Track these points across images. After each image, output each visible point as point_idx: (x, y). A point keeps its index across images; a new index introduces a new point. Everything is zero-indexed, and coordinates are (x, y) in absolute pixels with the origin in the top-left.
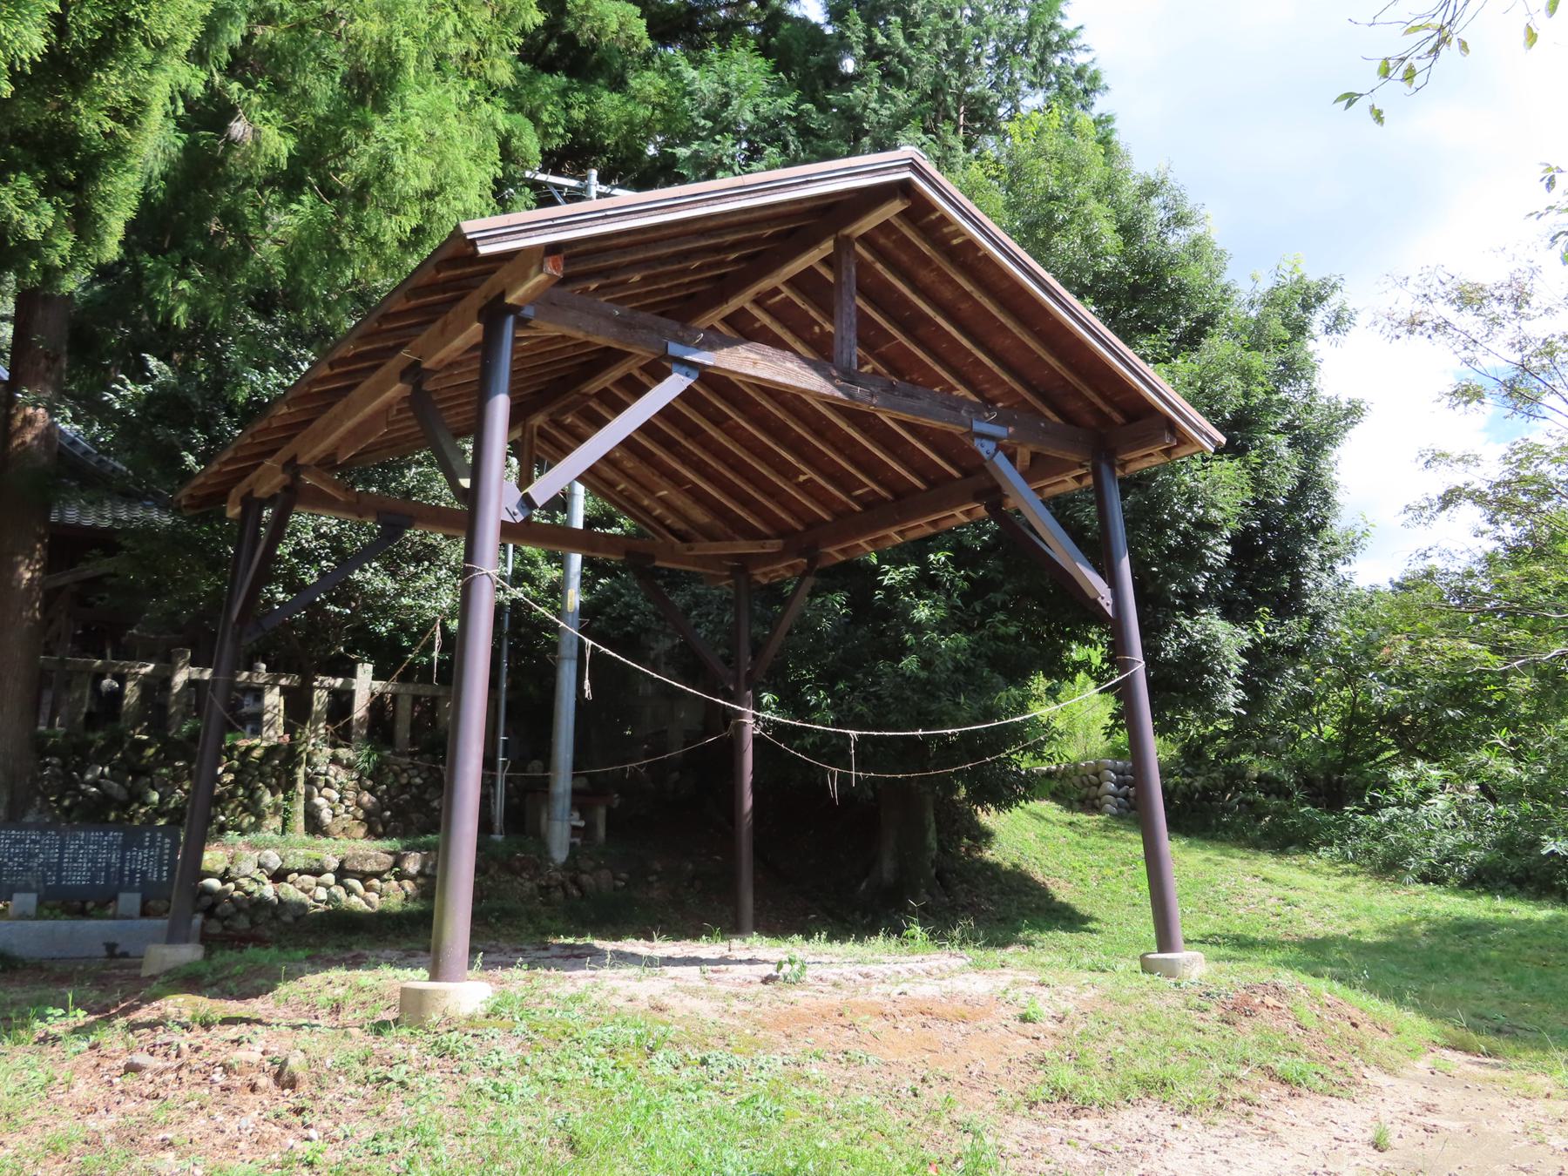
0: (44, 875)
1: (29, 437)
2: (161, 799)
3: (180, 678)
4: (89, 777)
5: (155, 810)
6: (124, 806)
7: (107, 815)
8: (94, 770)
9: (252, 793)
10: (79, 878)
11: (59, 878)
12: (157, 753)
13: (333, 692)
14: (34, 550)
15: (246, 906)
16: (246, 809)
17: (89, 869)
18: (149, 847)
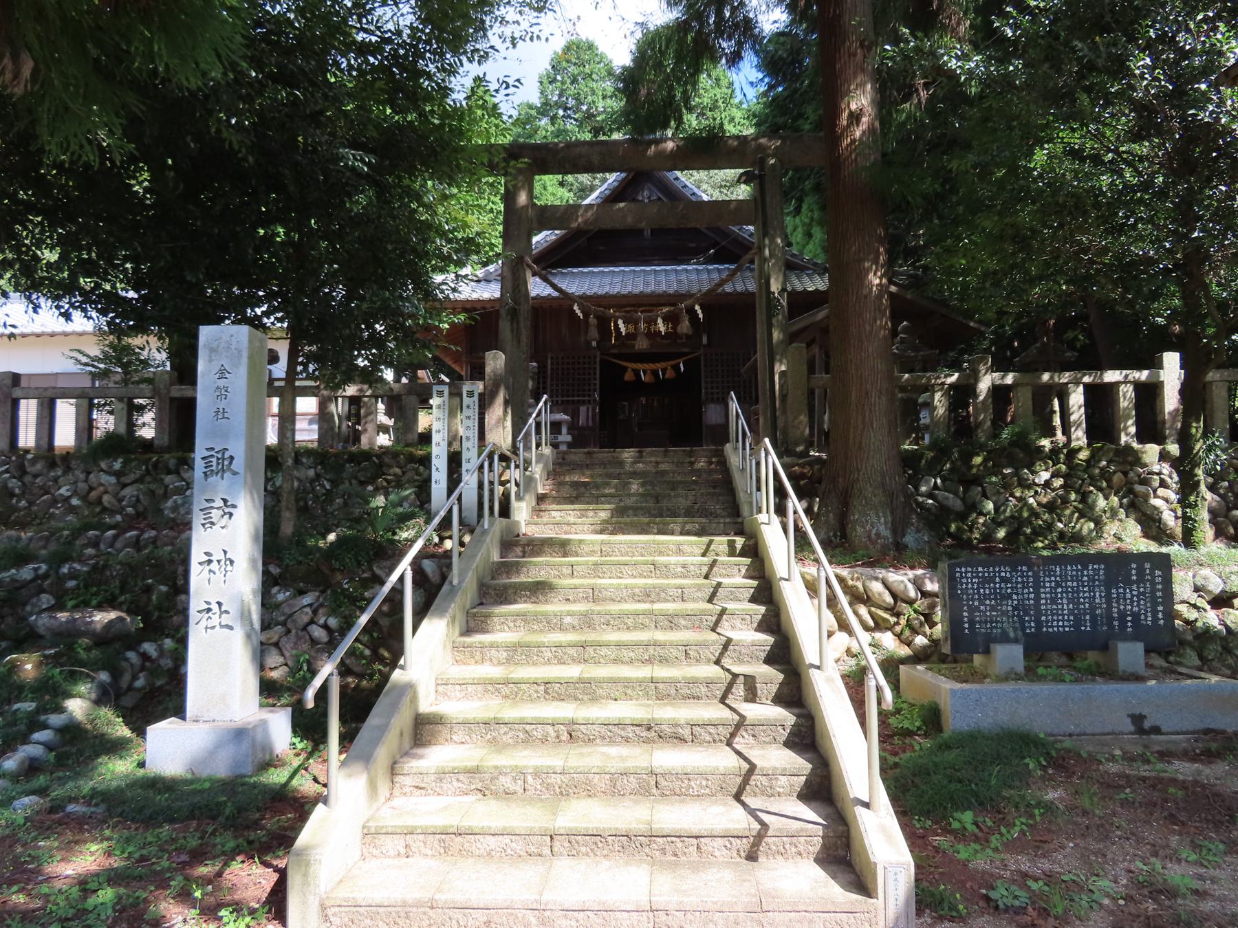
0: (1022, 622)
1: (858, 134)
2: (997, 509)
3: (985, 384)
4: (923, 489)
5: (993, 520)
6: (962, 517)
7: (948, 528)
8: (927, 482)
9: (1084, 497)
10: (1060, 624)
11: (1039, 624)
12: (985, 460)
13: (1139, 386)
14: (878, 254)
15: (1190, 637)
16: (1082, 516)
17: (1071, 612)
18: (1138, 582)
